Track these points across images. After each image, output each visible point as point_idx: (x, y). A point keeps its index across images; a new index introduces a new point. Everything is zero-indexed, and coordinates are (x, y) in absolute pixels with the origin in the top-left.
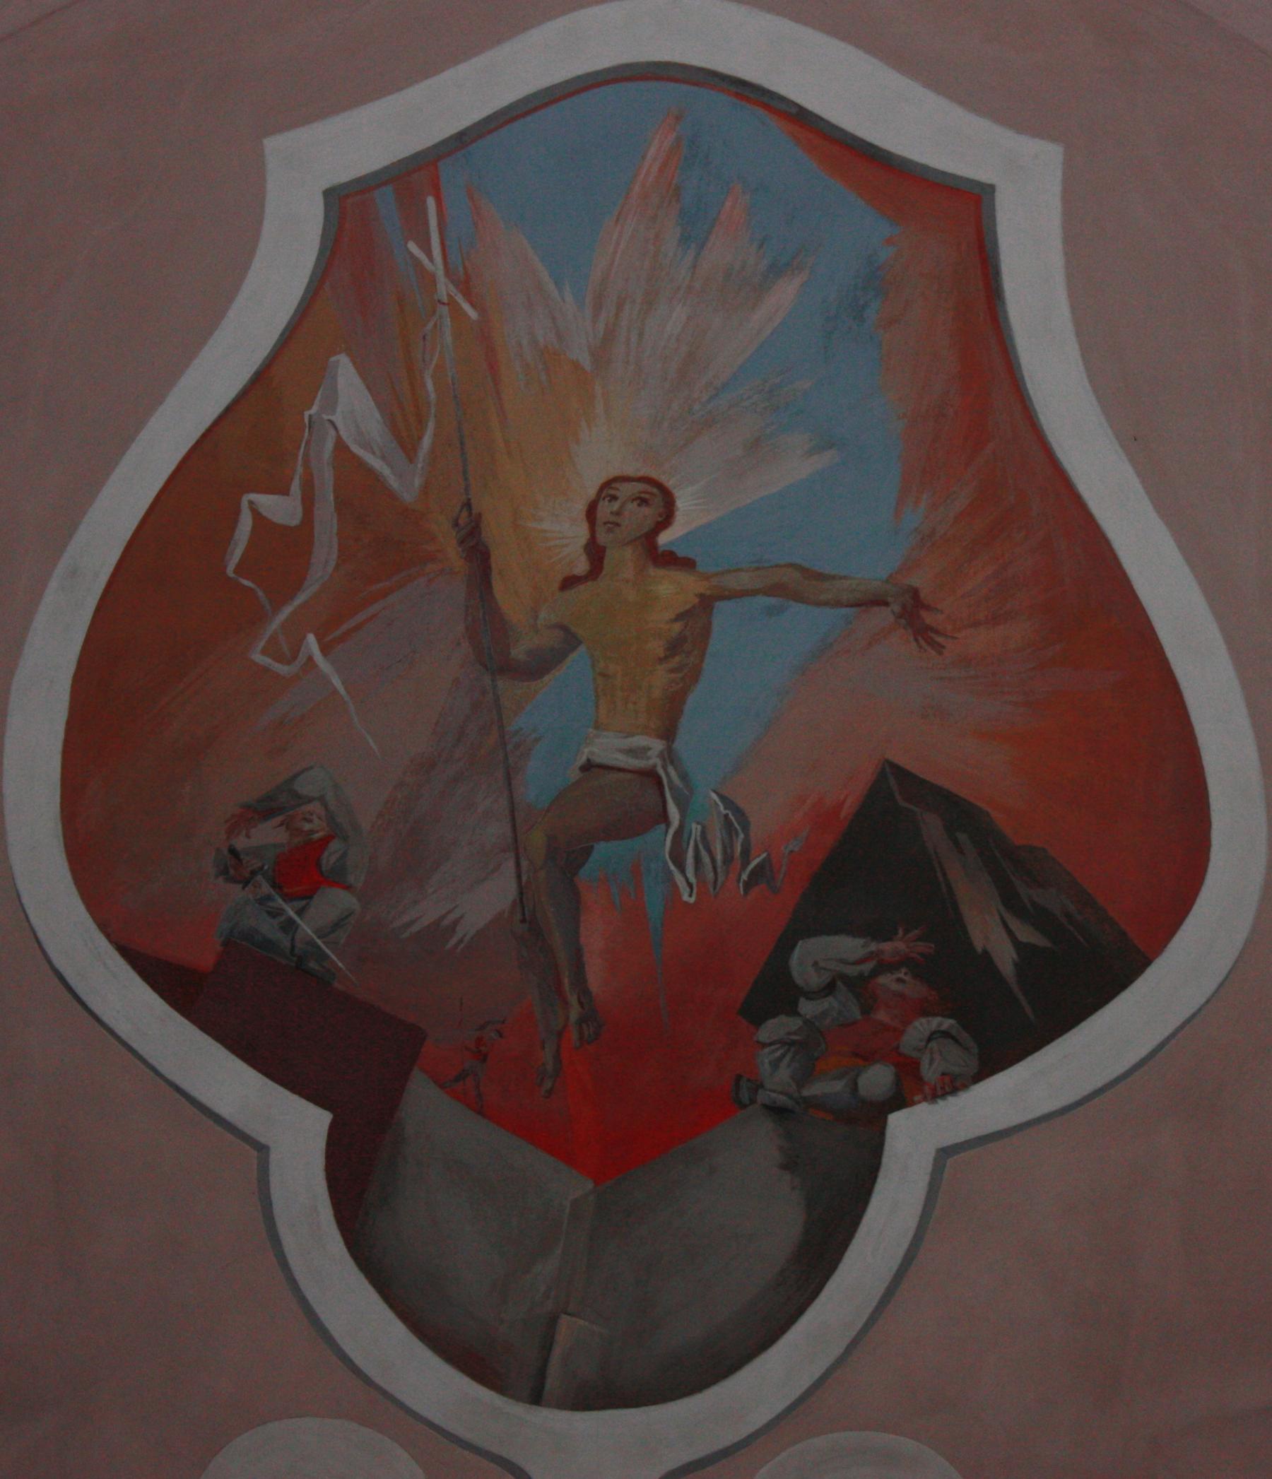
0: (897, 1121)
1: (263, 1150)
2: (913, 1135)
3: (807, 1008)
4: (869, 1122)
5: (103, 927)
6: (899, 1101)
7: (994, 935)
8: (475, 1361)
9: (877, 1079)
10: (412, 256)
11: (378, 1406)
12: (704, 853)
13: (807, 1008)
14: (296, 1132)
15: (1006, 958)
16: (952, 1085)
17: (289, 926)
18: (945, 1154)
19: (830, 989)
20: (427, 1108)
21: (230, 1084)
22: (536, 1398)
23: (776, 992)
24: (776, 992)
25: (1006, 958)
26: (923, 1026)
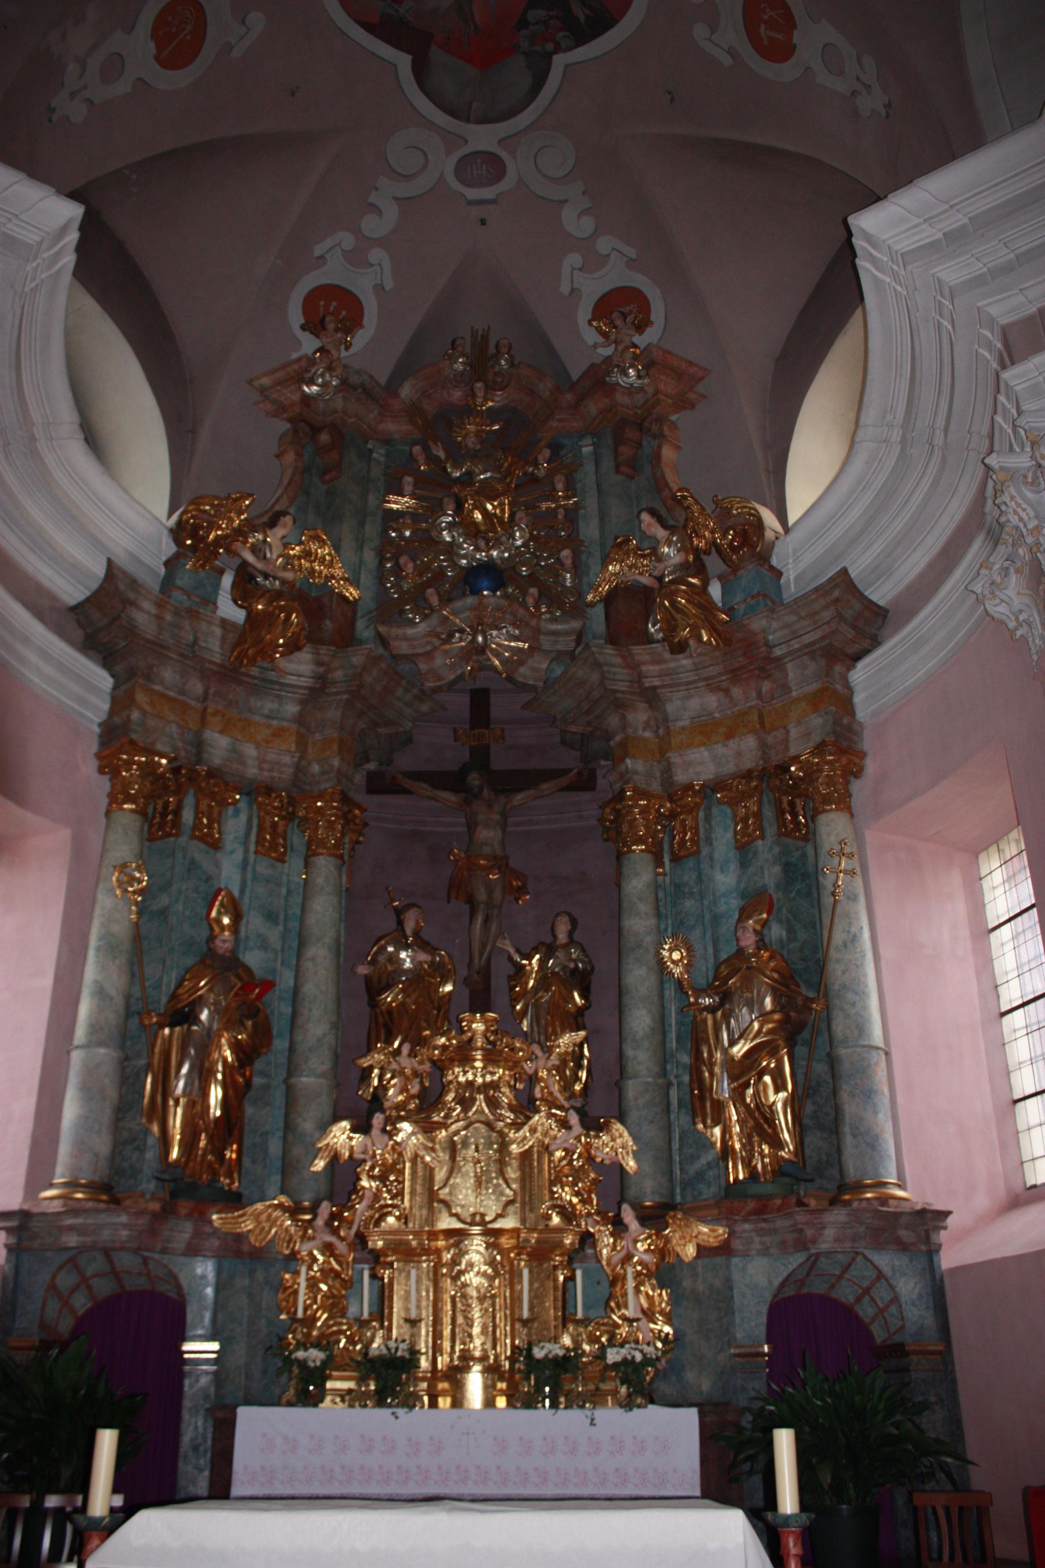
0: (555, 57)
1: (395, 66)
2: (559, 61)
3: (532, 28)
4: (548, 57)
5: (350, 15)
6: (555, 52)
7: (580, 12)
8: (452, 113)
9: (550, 47)
10: (411, 1200)
11: (429, 124)
12: (476, 945)
13: (532, 28)
14: (404, 61)
15: (582, 18)
16: (569, 49)
17: (397, 11)
18: (566, 66)
19: (537, 23)
20: (436, 53)
21: (386, 51)
22: (468, 121)
23: (523, 23)
24: (523, 23)
25: (582, 18)
26: (562, 34)
